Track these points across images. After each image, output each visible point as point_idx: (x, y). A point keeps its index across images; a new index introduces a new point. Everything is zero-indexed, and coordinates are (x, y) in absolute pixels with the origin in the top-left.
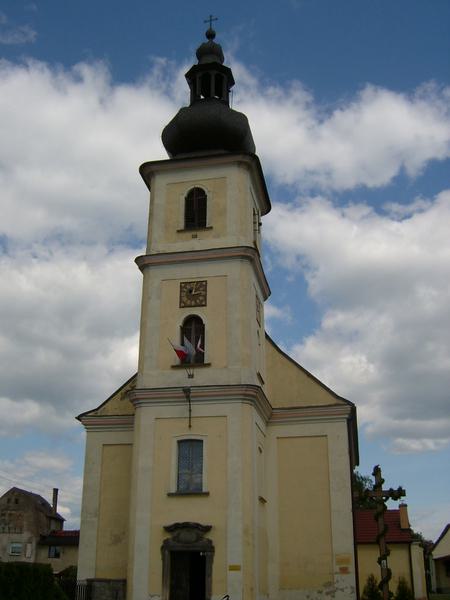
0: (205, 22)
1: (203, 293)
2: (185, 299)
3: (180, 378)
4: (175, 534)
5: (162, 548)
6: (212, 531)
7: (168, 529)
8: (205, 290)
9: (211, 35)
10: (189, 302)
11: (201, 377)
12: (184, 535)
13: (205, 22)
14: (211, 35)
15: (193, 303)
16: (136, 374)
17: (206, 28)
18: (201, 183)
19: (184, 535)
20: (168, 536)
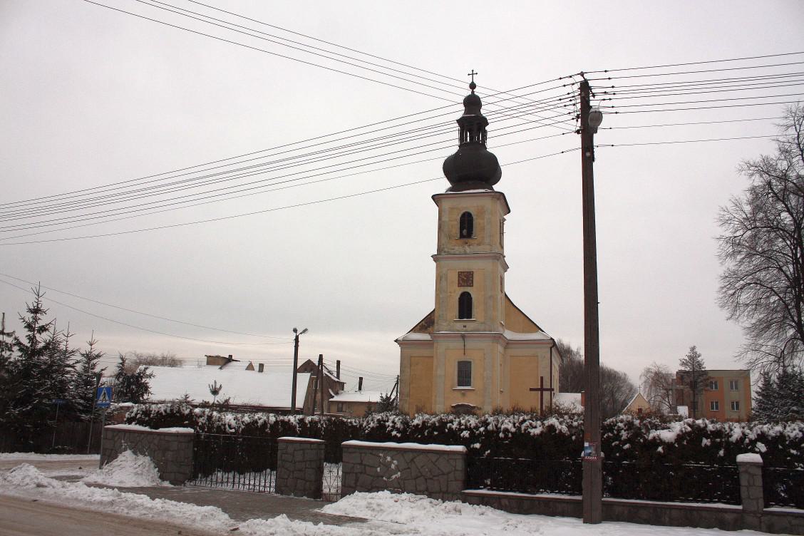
9: (473, 86)
11: (470, 326)
14: (473, 86)
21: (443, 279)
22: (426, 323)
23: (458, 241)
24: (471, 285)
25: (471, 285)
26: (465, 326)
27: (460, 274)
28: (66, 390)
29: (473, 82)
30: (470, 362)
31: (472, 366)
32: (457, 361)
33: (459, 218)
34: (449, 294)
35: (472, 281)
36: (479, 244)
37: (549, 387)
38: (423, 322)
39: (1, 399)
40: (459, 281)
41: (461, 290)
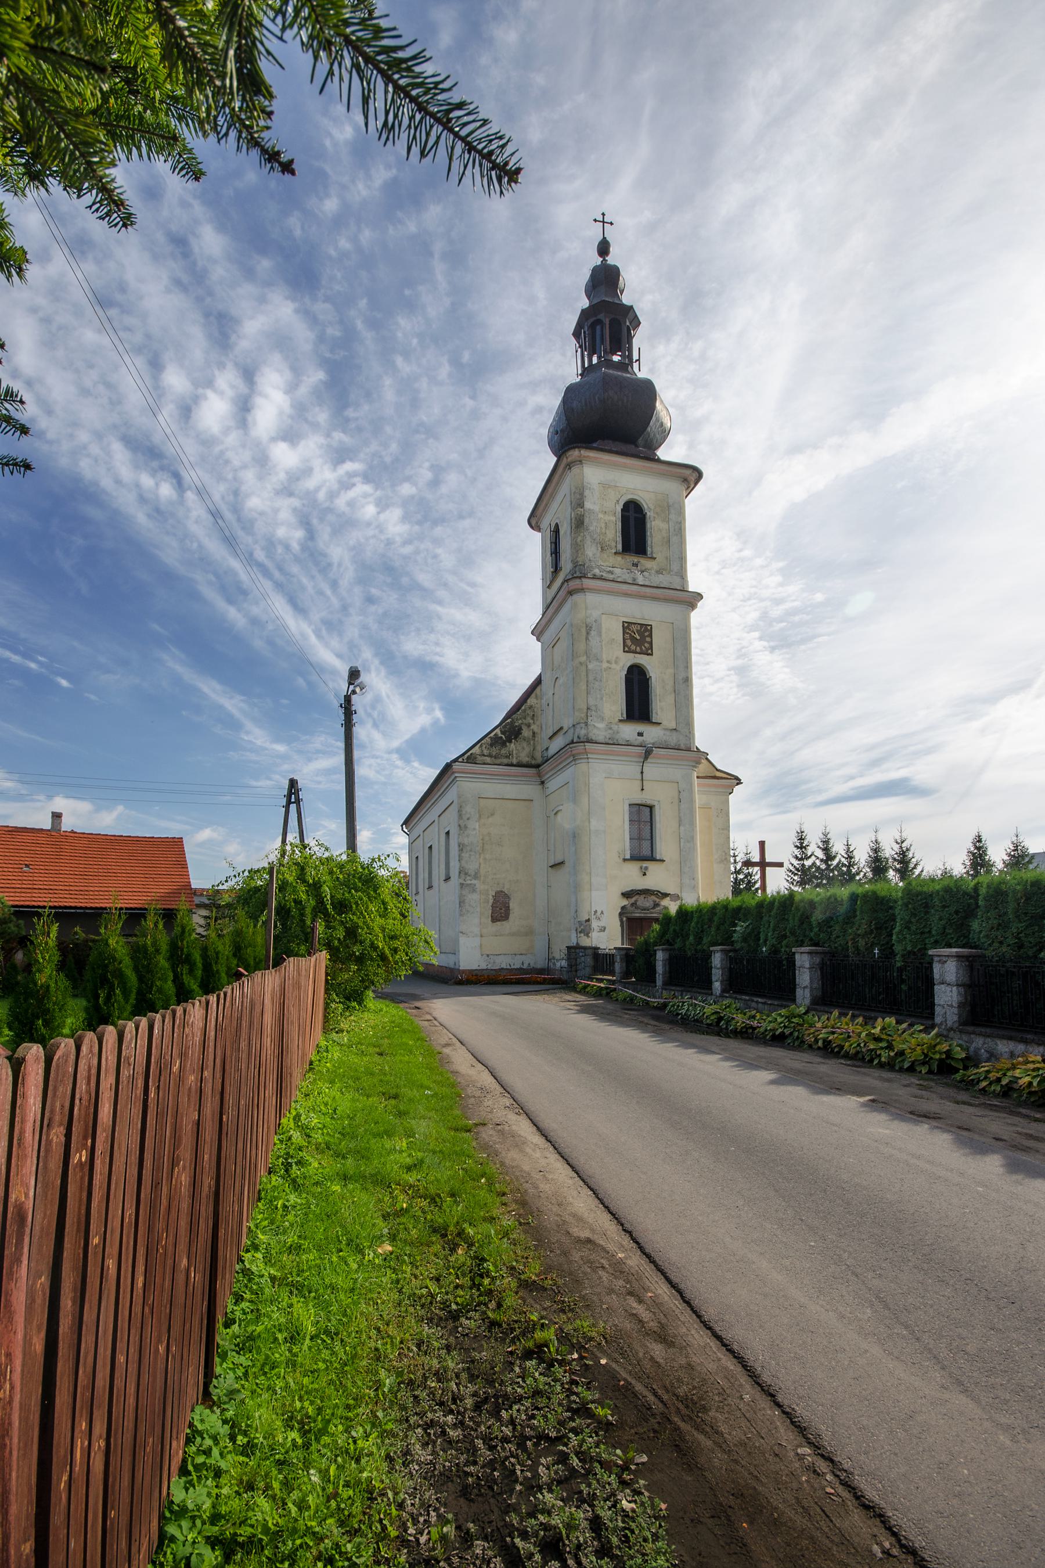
0: (603, 214)
1: (648, 639)
2: (629, 642)
3: (629, 731)
4: (633, 900)
5: (620, 914)
6: (522, 172)
7: (626, 895)
8: (651, 636)
9: (604, 248)
10: (633, 647)
11: (652, 734)
12: (644, 902)
13: (603, 214)
14: (604, 248)
15: (638, 649)
16: (538, 682)
17: (595, 234)
18: (640, 493)
19: (644, 902)
20: (625, 902)
21: (593, 633)
22: (502, 733)
23: (619, 558)
24: (649, 652)
25: (649, 652)
26: (640, 734)
27: (627, 626)
28: (866, 1024)
29: (604, 238)
30: (180, 840)
31: (187, 849)
32: (656, 803)
33: (619, 508)
34: (605, 665)
35: (651, 643)
36: (659, 572)
37: (649, 853)
38: (498, 731)
39: (338, 7)
40: (624, 640)
41: (630, 659)
